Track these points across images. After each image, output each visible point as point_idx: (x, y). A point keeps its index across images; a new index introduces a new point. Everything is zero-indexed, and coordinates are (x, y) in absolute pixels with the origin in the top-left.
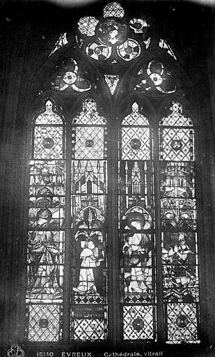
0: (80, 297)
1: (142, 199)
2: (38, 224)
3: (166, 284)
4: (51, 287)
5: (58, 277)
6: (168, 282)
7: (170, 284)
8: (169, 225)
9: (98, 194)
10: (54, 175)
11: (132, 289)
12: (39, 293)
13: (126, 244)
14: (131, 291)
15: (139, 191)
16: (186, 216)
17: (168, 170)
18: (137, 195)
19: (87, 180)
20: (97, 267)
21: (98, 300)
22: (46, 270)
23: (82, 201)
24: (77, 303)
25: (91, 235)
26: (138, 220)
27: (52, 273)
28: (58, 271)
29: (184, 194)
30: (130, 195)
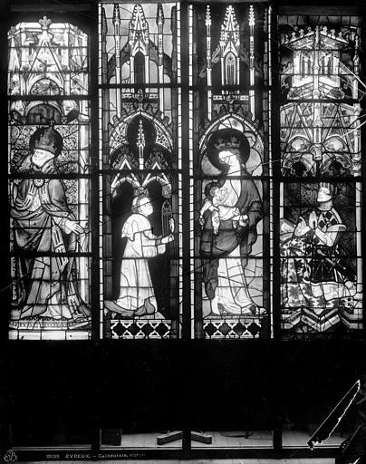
0: (123, 322)
1: (243, 98)
2: (33, 164)
3: (291, 298)
4: (62, 302)
5: (77, 281)
6: (295, 293)
7: (301, 297)
8: (300, 167)
9: (158, 86)
10: (64, 48)
11: (220, 306)
12: (38, 317)
13: (207, 206)
14: (216, 311)
15: (237, 79)
16: (337, 145)
17: (298, 35)
18: (231, 88)
19: (134, 54)
20: (159, 256)
21: (161, 329)
22: (50, 266)
23: (123, 100)
24: (116, 336)
25: (146, 182)
26: (234, 148)
27: (64, 273)
28: (75, 271)
29: (334, 91)
30: (217, 89)
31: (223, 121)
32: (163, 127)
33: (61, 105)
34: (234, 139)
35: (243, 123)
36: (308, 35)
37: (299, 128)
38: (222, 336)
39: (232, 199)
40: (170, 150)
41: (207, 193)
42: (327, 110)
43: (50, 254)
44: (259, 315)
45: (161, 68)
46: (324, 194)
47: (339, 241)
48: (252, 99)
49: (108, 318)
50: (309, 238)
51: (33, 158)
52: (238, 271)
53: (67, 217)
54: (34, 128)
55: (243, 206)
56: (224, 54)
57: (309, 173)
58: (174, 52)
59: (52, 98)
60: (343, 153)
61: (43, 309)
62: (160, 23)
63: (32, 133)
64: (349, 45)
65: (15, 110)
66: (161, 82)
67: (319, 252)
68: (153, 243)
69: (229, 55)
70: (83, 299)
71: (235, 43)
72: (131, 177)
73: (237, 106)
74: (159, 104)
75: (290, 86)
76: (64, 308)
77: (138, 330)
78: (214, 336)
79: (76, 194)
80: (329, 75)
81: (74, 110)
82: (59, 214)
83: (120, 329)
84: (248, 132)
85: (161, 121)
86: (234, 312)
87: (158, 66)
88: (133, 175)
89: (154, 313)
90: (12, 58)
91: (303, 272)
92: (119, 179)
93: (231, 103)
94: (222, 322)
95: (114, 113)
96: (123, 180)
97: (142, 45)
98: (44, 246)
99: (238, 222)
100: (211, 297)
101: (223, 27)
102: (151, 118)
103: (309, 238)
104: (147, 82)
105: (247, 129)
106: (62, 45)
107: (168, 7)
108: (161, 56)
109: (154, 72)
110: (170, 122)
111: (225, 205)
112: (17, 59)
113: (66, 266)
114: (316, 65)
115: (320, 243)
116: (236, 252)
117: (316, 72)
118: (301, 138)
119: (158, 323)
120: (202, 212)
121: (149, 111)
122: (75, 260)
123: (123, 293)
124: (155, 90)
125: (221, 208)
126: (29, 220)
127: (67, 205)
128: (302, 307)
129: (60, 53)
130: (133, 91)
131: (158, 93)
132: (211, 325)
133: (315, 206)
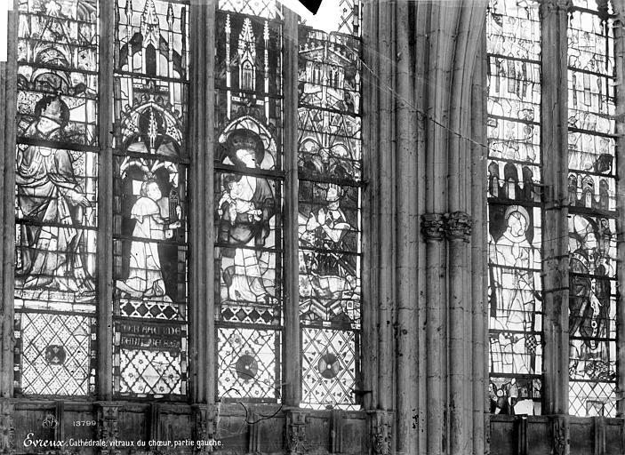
0: (132, 303)
1: (259, 102)
2: (38, 131)
5: (84, 254)
9: (167, 79)
11: (237, 293)
12: (43, 287)
13: (226, 197)
14: (233, 297)
18: (249, 92)
21: (169, 311)
22: (57, 238)
23: (135, 90)
27: (71, 245)
28: (83, 244)
31: (240, 121)
32: (173, 119)
33: (68, 76)
34: (250, 140)
35: (259, 127)
36: (318, 48)
37: (311, 131)
38: (238, 321)
39: (249, 195)
40: (179, 143)
41: (226, 184)
42: (334, 119)
43: (55, 223)
44: (272, 304)
45: (171, 64)
46: (333, 193)
47: (342, 239)
48: (267, 105)
49: (116, 298)
50: (319, 233)
51: (39, 126)
52: (253, 261)
53: (74, 189)
54: (41, 96)
55: (258, 201)
56: (242, 61)
57: (318, 172)
58: (184, 51)
59: (61, 68)
60: (347, 160)
61: (49, 279)
62: (170, 21)
63: (38, 100)
64: (352, 64)
65: (21, 76)
66: (171, 76)
67: (326, 245)
68: (161, 228)
69: (245, 64)
70: (91, 272)
71: (251, 53)
72: (140, 161)
73: (253, 109)
74: (169, 98)
75: (303, 92)
76: (71, 281)
77: (146, 311)
78: (231, 320)
79: (83, 167)
80: (336, 89)
81: (81, 84)
82: (67, 185)
83: (129, 309)
84: (263, 134)
85: (172, 114)
86: (249, 300)
87: (168, 61)
88: (142, 159)
89: (162, 296)
90: (21, 25)
91: (312, 264)
92: (128, 162)
93: (249, 105)
94: (239, 308)
95: (124, 103)
96: (132, 163)
97: (153, 38)
98: (48, 216)
99: (253, 216)
100: (228, 285)
101: (241, 37)
102: (162, 110)
103: (319, 233)
104: (158, 74)
105: (262, 132)
106: (70, 17)
107: (178, 8)
108: (171, 52)
109: (164, 66)
110: (180, 116)
111: (242, 195)
112: (27, 25)
113: (74, 238)
114: (325, 76)
115: (327, 238)
116: (251, 244)
117: (325, 83)
118: (313, 141)
119: (166, 305)
120: (221, 203)
121: (161, 103)
122: (83, 233)
123: (133, 274)
124: (166, 84)
125: (239, 202)
126: (34, 187)
127: (74, 177)
128: (312, 297)
129: (69, 26)
130: (144, 82)
131: (168, 87)
132: (228, 310)
133: (325, 205)
